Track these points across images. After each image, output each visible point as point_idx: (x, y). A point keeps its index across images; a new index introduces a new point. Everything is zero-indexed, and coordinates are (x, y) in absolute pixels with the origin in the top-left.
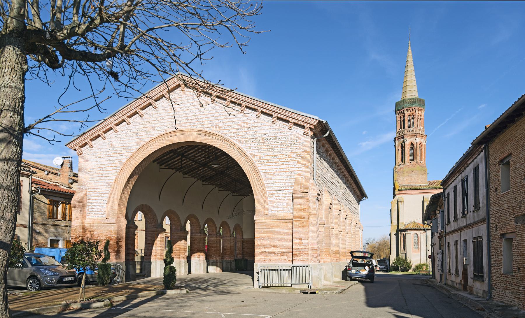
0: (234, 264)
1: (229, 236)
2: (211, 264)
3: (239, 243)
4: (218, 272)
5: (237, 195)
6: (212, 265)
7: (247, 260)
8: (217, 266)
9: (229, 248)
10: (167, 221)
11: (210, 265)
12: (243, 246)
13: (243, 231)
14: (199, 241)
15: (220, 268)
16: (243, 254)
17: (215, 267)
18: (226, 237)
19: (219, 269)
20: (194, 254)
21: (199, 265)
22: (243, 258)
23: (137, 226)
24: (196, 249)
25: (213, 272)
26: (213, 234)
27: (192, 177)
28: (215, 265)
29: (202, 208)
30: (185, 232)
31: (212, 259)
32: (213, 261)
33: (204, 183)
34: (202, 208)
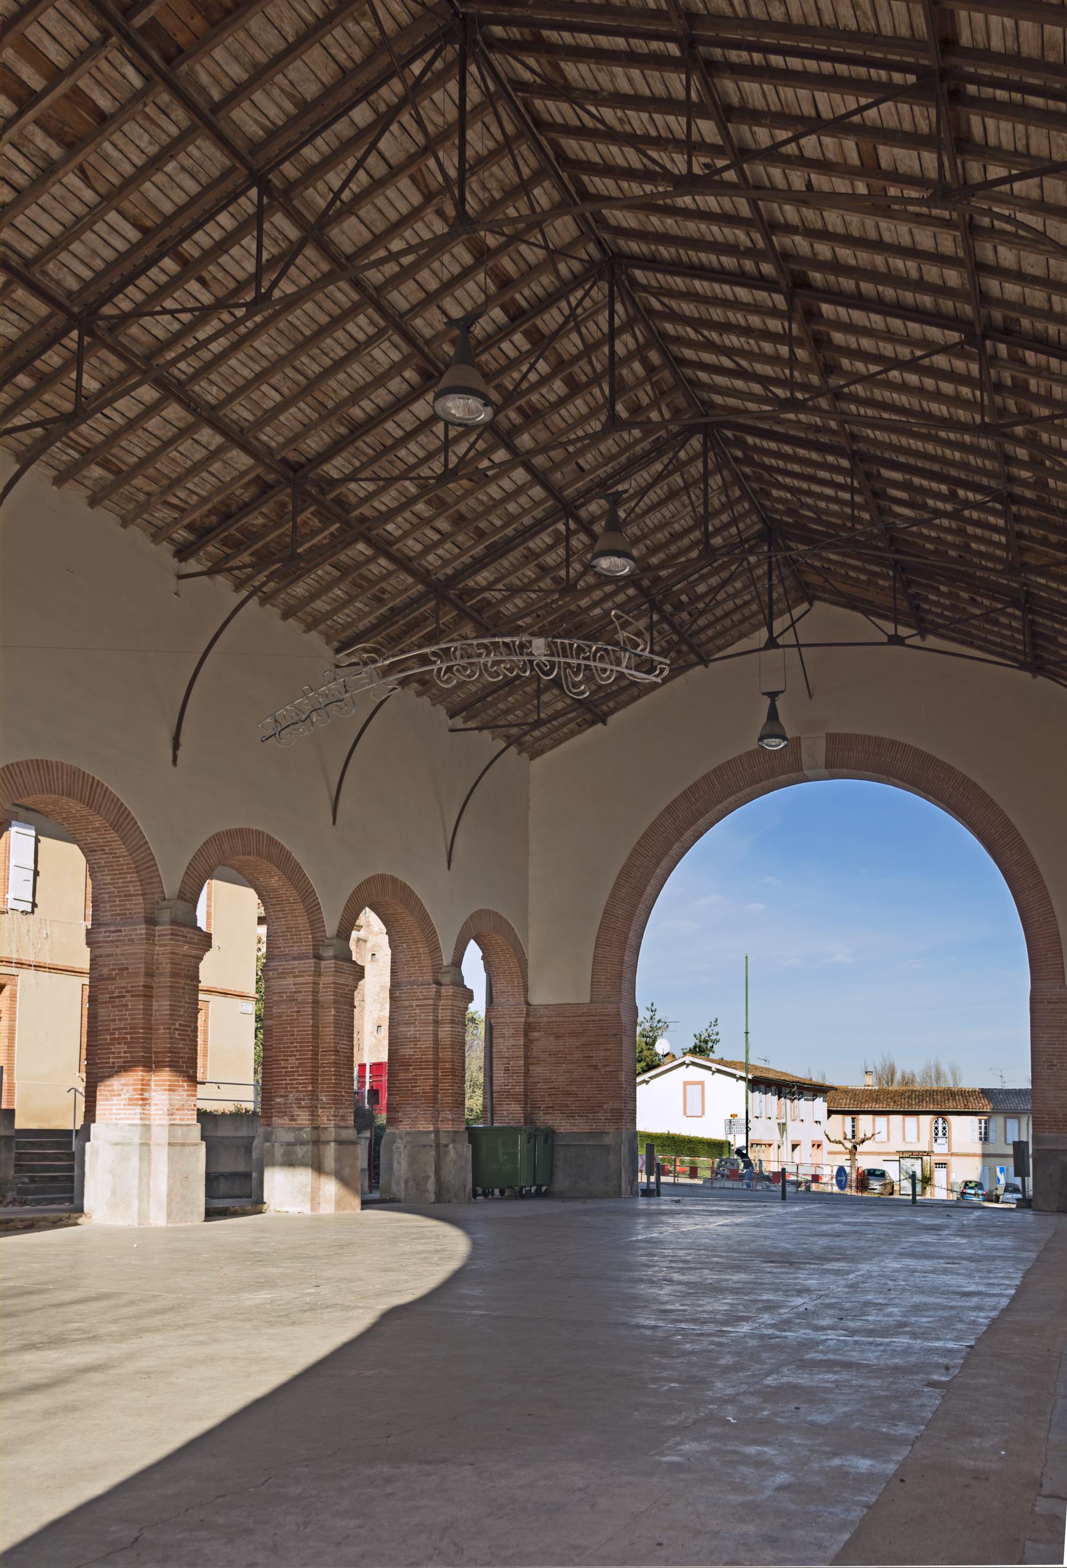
0: (461, 1154)
1: (429, 978)
2: (279, 1151)
3: (508, 1031)
4: (327, 1209)
5: (471, 724)
6: (290, 1162)
7: (550, 1134)
8: (318, 1168)
9: (430, 1057)
10: (473, 957)
11: (273, 1164)
12: (527, 1047)
13: (530, 956)
14: (141, 981)
15: (344, 1181)
16: (527, 1099)
17: (304, 1176)
18: (412, 983)
19: (330, 1187)
20: (108, 1083)
21: (135, 1162)
22: (529, 1119)
23: (471, 991)
24: (119, 1040)
25: (293, 1210)
26: (295, 951)
27: (480, 729)
28: (303, 1164)
29: (176, 745)
30: (346, 965)
31: (286, 1121)
32: (290, 1137)
33: (458, 722)
34: (176, 745)
